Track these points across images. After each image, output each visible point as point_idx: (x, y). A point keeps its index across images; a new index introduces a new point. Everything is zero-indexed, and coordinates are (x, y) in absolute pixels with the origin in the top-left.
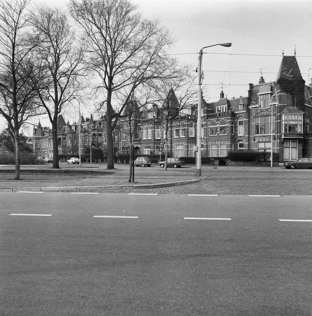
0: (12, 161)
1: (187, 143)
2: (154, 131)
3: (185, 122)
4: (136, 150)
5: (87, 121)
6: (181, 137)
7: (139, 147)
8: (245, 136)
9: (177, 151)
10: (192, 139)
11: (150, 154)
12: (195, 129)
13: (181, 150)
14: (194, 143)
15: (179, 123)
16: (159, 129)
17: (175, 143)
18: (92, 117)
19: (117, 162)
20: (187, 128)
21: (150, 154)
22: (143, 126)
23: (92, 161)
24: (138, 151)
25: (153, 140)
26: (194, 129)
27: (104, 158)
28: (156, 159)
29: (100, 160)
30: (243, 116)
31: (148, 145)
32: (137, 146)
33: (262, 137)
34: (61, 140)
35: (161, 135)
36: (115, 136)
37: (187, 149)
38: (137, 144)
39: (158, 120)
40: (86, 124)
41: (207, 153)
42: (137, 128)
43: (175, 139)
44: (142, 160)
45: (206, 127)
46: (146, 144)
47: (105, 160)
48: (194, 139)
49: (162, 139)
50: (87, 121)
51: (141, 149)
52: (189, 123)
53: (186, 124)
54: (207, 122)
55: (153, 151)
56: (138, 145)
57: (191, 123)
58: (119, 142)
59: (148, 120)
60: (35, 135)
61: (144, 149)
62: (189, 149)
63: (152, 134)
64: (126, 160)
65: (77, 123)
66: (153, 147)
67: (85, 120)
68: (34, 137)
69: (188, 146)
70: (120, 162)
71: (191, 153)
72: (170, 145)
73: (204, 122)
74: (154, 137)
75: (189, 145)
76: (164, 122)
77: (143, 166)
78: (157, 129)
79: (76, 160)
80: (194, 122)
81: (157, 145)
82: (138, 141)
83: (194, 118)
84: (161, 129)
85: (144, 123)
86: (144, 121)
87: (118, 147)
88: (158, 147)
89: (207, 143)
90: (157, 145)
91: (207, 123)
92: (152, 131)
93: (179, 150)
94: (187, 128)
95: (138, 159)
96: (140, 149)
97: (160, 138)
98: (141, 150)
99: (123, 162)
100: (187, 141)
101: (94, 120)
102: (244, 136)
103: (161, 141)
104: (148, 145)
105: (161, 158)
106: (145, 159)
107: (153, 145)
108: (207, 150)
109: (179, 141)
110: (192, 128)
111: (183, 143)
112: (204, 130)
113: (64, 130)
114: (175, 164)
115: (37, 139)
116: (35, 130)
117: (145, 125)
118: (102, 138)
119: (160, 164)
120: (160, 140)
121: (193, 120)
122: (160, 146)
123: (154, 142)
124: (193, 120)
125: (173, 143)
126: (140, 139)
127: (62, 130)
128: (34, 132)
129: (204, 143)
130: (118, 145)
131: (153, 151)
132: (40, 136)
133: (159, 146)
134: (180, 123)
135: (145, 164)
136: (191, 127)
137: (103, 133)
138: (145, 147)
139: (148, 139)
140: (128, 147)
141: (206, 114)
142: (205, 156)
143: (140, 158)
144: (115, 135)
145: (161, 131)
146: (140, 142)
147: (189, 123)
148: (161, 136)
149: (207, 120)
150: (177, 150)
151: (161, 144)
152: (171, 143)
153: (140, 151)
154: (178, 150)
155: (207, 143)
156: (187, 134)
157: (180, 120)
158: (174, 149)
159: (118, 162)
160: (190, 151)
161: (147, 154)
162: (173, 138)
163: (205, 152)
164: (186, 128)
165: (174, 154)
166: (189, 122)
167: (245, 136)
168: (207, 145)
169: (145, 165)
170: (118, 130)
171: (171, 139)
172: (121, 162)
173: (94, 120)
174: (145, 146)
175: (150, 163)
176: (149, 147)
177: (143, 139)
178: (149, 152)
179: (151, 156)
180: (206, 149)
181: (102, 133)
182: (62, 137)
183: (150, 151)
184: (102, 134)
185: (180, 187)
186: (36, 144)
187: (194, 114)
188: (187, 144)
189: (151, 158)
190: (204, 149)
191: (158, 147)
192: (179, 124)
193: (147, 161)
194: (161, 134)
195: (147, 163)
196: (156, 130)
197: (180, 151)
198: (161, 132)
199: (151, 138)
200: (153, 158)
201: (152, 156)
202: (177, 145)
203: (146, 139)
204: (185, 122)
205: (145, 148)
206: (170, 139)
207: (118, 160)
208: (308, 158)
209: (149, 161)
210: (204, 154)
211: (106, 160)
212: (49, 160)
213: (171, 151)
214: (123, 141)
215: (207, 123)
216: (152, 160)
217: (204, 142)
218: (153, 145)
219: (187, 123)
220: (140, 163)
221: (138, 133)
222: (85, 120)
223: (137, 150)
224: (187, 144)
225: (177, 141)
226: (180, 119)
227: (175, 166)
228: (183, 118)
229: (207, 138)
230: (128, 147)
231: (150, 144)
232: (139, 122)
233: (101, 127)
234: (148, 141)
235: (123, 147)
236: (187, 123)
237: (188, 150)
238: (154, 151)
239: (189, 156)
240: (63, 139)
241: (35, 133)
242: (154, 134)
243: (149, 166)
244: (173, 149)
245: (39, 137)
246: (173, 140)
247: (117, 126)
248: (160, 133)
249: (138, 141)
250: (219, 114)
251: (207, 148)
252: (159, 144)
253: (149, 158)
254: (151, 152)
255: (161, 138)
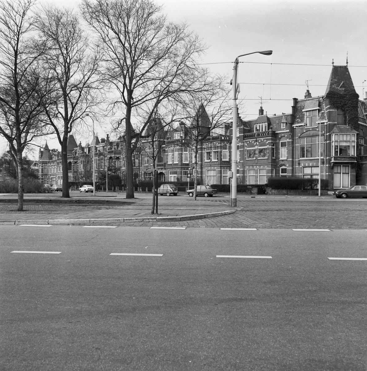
0: (14, 189)
1: (220, 167)
2: (182, 154)
3: (217, 144)
4: (160, 177)
5: (102, 142)
6: (213, 160)
7: (163, 172)
8: (288, 160)
9: (209, 177)
10: (225, 163)
11: (176, 181)
12: (229, 152)
13: (213, 176)
14: (228, 167)
15: (210, 145)
16: (187, 152)
17: (206, 168)
18: (108, 137)
19: (137, 191)
20: (220, 150)
21: (176, 181)
22: (168, 148)
23: (109, 189)
24: (162, 177)
25: (180, 164)
26: (228, 151)
27: (123, 186)
28: (183, 187)
29: (118, 187)
30: (286, 136)
31: (174, 170)
32: (161, 171)
33: (308, 160)
34: (72, 164)
35: (189, 158)
36: (136, 160)
37: (220, 175)
38: (162, 169)
39: (186, 141)
40: (102, 146)
41: (243, 179)
42: (162, 150)
43: (205, 163)
44: (167, 188)
45: (242, 149)
46: (171, 169)
47: (123, 187)
48: (228, 163)
49: (191, 163)
50: (102, 142)
51: (166, 175)
52: (222, 144)
53: (219, 146)
54: (243, 143)
55: (180, 178)
56: (163, 170)
57: (225, 145)
58: (140, 167)
59: (174, 140)
60: (41, 158)
61: (170, 175)
62: (223, 175)
63: (179, 157)
64: (148, 188)
65: (90, 144)
66: (180, 172)
67: (100, 141)
68: (40, 161)
69: (221, 171)
70: (141, 190)
71: (225, 180)
72: (200, 170)
73: (240, 143)
74: (182, 160)
75: (222, 170)
76: (193, 144)
77: (168, 194)
78: (184, 151)
79: (90, 188)
80: (229, 144)
81: (185, 171)
82: (162, 165)
83: (228, 138)
84: (189, 152)
85: (169, 144)
86: (170, 142)
87: (138, 172)
88: (186, 172)
89: (243, 168)
90: (185, 170)
91: (243, 145)
92: (179, 153)
93: (211, 176)
94: (220, 150)
95: (162, 186)
96: (164, 175)
97: (188, 162)
98: (166, 176)
99: (145, 190)
100: (220, 166)
101: (110, 141)
102: (287, 160)
103: (189, 165)
104: (174, 170)
105: (189, 186)
106: (171, 187)
107: (180, 170)
108: (243, 176)
109: (211, 166)
110: (226, 150)
111: (216, 168)
112: (240, 152)
113: (76, 153)
114: (206, 193)
115: (43, 163)
116: (41, 152)
117: (171, 147)
118: (120, 162)
119: (188, 192)
120: (188, 165)
121: (227, 141)
122: (188, 171)
123: (181, 167)
124: (227, 141)
125: (204, 168)
126: (165, 163)
127: (74, 153)
128: (40, 155)
129: (240, 168)
130: (138, 170)
131: (180, 178)
132: (47, 160)
133: (187, 171)
134: (212, 144)
135: (170, 192)
136: (225, 149)
137: (122, 157)
138: (170, 172)
139: (175, 163)
140: (150, 172)
141: (243, 134)
142: (241, 184)
143: (165, 186)
144: (135, 159)
145: (189, 153)
146: (165, 166)
147: (222, 144)
148: (189, 160)
149: (244, 141)
150: (208, 176)
151: (190, 169)
152: (202, 168)
153: (165, 177)
154: (210, 176)
155: (243, 168)
156: (221, 157)
157: (212, 141)
158: (204, 175)
159: (138, 190)
160: (224, 177)
161: (173, 181)
162: (203, 162)
163: (242, 179)
164: (219, 150)
165: (205, 181)
166: (222, 143)
167: (288, 160)
168: (243, 170)
169: (170, 193)
170: (138, 153)
171: (202, 163)
172: (142, 190)
173: (110, 141)
174: (170, 172)
175: (176, 192)
176: (175, 173)
177: (169, 163)
178: (176, 179)
179: (177, 183)
180: (242, 175)
181: (120, 156)
182: (73, 161)
183: (176, 177)
184: (120, 158)
185: (212, 220)
186: (42, 169)
187: (228, 134)
188: (220, 169)
189: (177, 185)
190: (240, 175)
191: (186, 172)
192: (211, 145)
193: (173, 189)
194: (189, 157)
195: (173, 191)
196: (184, 152)
197: (212, 177)
198: (189, 155)
199: (177, 163)
200: (180, 185)
201: (178, 183)
202: (208, 171)
203: (171, 163)
204: (217, 144)
205: (170, 173)
206: (200, 163)
207: (138, 188)
208: (362, 185)
209: (175, 190)
210: (240, 181)
211: (124, 188)
212: (57, 188)
213: (202, 177)
214: (145, 165)
215: (243, 145)
216: (178, 188)
217: (240, 167)
218: (180, 170)
219: (220, 145)
220: (165, 192)
221: (162, 156)
222: (100, 141)
223: (161, 176)
224: (220, 169)
225: (208, 165)
226: (212, 140)
227: (206, 195)
228: (215, 139)
229: (243, 162)
230: (151, 173)
231: (177, 169)
232: (164, 143)
233: (119, 149)
234: (174, 166)
235: (145, 172)
236: (220, 145)
237: (221, 177)
238: (181, 177)
239: (222, 184)
240: (74, 163)
241: (42, 156)
242: (182, 158)
243: (175, 194)
244: (204, 175)
245: (46, 161)
246: (203, 164)
247: (138, 147)
248: (188, 156)
249: (162, 165)
250: (258, 134)
251: (243, 174)
252: (187, 170)
253: (176, 186)
254: (178, 179)
255: (189, 163)
